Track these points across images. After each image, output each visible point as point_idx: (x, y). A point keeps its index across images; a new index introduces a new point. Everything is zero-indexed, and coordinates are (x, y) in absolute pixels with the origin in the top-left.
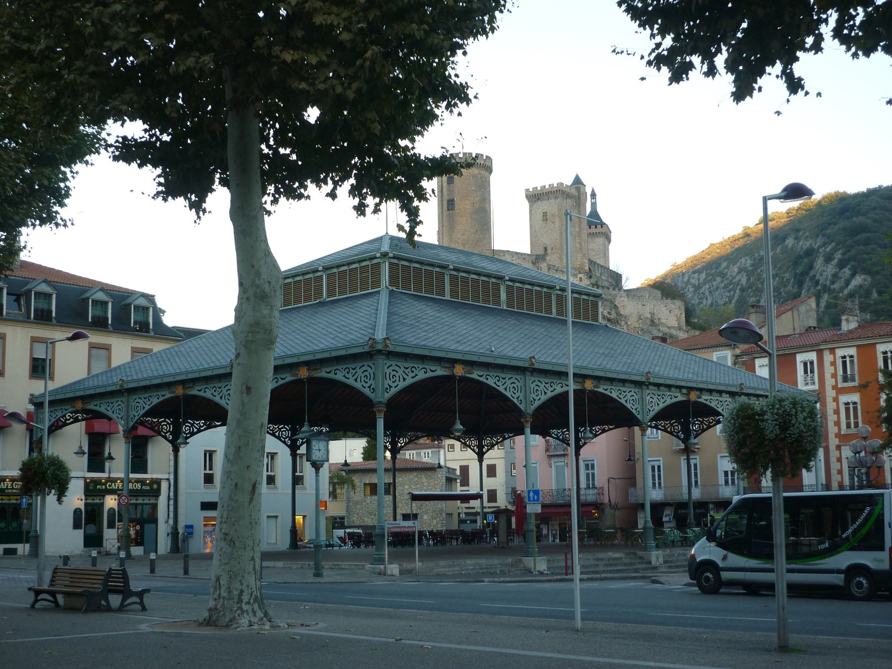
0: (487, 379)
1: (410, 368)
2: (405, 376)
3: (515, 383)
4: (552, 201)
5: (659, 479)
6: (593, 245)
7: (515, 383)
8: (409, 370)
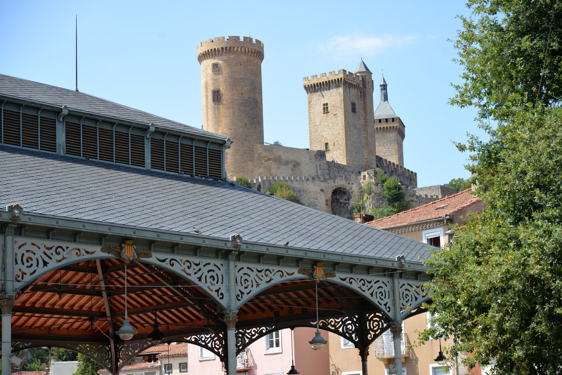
0: (351, 283)
1: (54, 249)
3: (213, 271)
7: (213, 271)
8: (53, 251)
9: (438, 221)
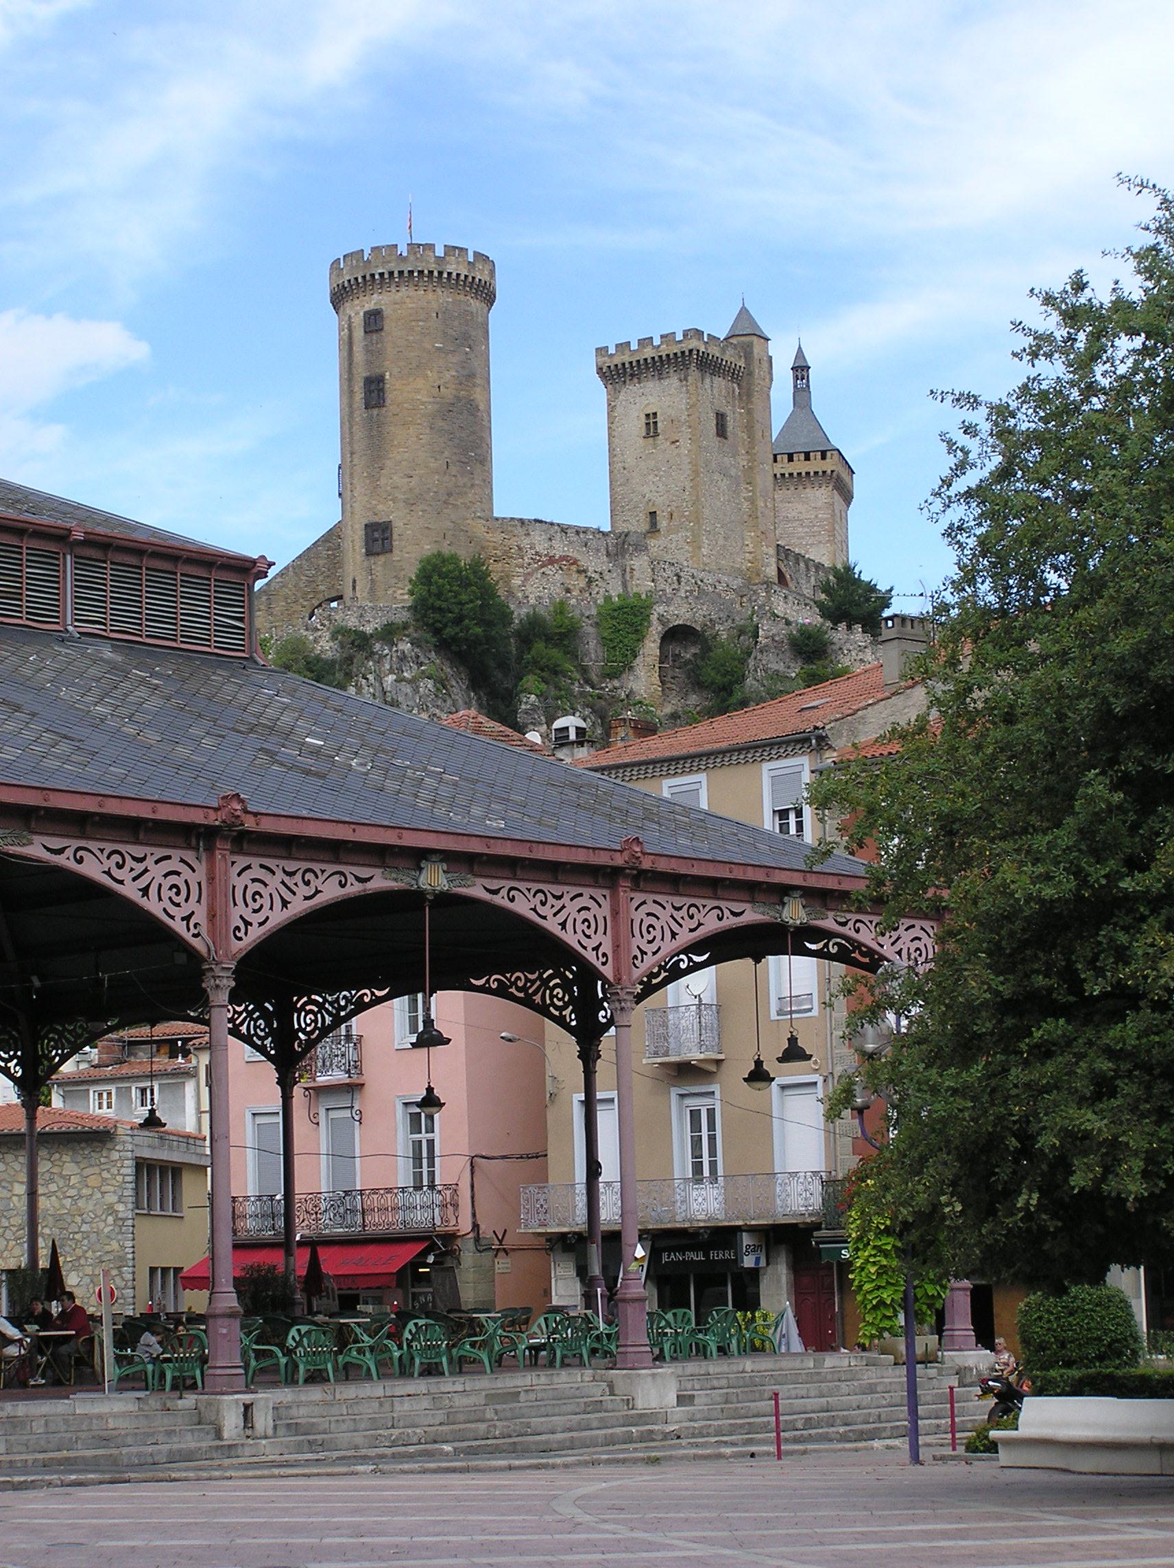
0: (857, 931)
1: (685, 908)
2: (287, 896)
3: (920, 939)
4: (673, 382)
5: (713, 1153)
6: (800, 507)
7: (920, 939)
8: (684, 912)
9: (797, 741)
